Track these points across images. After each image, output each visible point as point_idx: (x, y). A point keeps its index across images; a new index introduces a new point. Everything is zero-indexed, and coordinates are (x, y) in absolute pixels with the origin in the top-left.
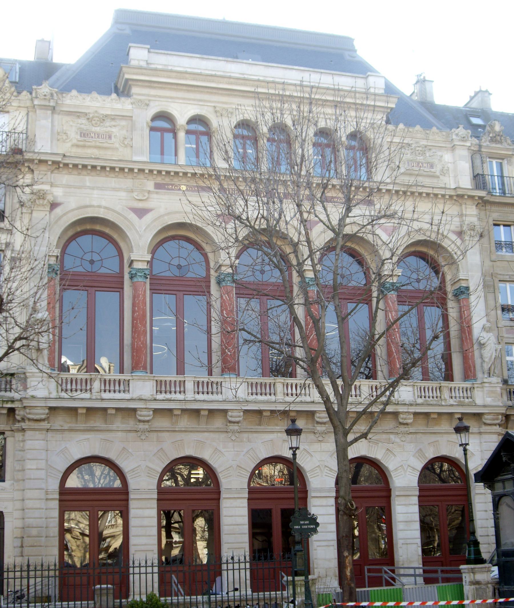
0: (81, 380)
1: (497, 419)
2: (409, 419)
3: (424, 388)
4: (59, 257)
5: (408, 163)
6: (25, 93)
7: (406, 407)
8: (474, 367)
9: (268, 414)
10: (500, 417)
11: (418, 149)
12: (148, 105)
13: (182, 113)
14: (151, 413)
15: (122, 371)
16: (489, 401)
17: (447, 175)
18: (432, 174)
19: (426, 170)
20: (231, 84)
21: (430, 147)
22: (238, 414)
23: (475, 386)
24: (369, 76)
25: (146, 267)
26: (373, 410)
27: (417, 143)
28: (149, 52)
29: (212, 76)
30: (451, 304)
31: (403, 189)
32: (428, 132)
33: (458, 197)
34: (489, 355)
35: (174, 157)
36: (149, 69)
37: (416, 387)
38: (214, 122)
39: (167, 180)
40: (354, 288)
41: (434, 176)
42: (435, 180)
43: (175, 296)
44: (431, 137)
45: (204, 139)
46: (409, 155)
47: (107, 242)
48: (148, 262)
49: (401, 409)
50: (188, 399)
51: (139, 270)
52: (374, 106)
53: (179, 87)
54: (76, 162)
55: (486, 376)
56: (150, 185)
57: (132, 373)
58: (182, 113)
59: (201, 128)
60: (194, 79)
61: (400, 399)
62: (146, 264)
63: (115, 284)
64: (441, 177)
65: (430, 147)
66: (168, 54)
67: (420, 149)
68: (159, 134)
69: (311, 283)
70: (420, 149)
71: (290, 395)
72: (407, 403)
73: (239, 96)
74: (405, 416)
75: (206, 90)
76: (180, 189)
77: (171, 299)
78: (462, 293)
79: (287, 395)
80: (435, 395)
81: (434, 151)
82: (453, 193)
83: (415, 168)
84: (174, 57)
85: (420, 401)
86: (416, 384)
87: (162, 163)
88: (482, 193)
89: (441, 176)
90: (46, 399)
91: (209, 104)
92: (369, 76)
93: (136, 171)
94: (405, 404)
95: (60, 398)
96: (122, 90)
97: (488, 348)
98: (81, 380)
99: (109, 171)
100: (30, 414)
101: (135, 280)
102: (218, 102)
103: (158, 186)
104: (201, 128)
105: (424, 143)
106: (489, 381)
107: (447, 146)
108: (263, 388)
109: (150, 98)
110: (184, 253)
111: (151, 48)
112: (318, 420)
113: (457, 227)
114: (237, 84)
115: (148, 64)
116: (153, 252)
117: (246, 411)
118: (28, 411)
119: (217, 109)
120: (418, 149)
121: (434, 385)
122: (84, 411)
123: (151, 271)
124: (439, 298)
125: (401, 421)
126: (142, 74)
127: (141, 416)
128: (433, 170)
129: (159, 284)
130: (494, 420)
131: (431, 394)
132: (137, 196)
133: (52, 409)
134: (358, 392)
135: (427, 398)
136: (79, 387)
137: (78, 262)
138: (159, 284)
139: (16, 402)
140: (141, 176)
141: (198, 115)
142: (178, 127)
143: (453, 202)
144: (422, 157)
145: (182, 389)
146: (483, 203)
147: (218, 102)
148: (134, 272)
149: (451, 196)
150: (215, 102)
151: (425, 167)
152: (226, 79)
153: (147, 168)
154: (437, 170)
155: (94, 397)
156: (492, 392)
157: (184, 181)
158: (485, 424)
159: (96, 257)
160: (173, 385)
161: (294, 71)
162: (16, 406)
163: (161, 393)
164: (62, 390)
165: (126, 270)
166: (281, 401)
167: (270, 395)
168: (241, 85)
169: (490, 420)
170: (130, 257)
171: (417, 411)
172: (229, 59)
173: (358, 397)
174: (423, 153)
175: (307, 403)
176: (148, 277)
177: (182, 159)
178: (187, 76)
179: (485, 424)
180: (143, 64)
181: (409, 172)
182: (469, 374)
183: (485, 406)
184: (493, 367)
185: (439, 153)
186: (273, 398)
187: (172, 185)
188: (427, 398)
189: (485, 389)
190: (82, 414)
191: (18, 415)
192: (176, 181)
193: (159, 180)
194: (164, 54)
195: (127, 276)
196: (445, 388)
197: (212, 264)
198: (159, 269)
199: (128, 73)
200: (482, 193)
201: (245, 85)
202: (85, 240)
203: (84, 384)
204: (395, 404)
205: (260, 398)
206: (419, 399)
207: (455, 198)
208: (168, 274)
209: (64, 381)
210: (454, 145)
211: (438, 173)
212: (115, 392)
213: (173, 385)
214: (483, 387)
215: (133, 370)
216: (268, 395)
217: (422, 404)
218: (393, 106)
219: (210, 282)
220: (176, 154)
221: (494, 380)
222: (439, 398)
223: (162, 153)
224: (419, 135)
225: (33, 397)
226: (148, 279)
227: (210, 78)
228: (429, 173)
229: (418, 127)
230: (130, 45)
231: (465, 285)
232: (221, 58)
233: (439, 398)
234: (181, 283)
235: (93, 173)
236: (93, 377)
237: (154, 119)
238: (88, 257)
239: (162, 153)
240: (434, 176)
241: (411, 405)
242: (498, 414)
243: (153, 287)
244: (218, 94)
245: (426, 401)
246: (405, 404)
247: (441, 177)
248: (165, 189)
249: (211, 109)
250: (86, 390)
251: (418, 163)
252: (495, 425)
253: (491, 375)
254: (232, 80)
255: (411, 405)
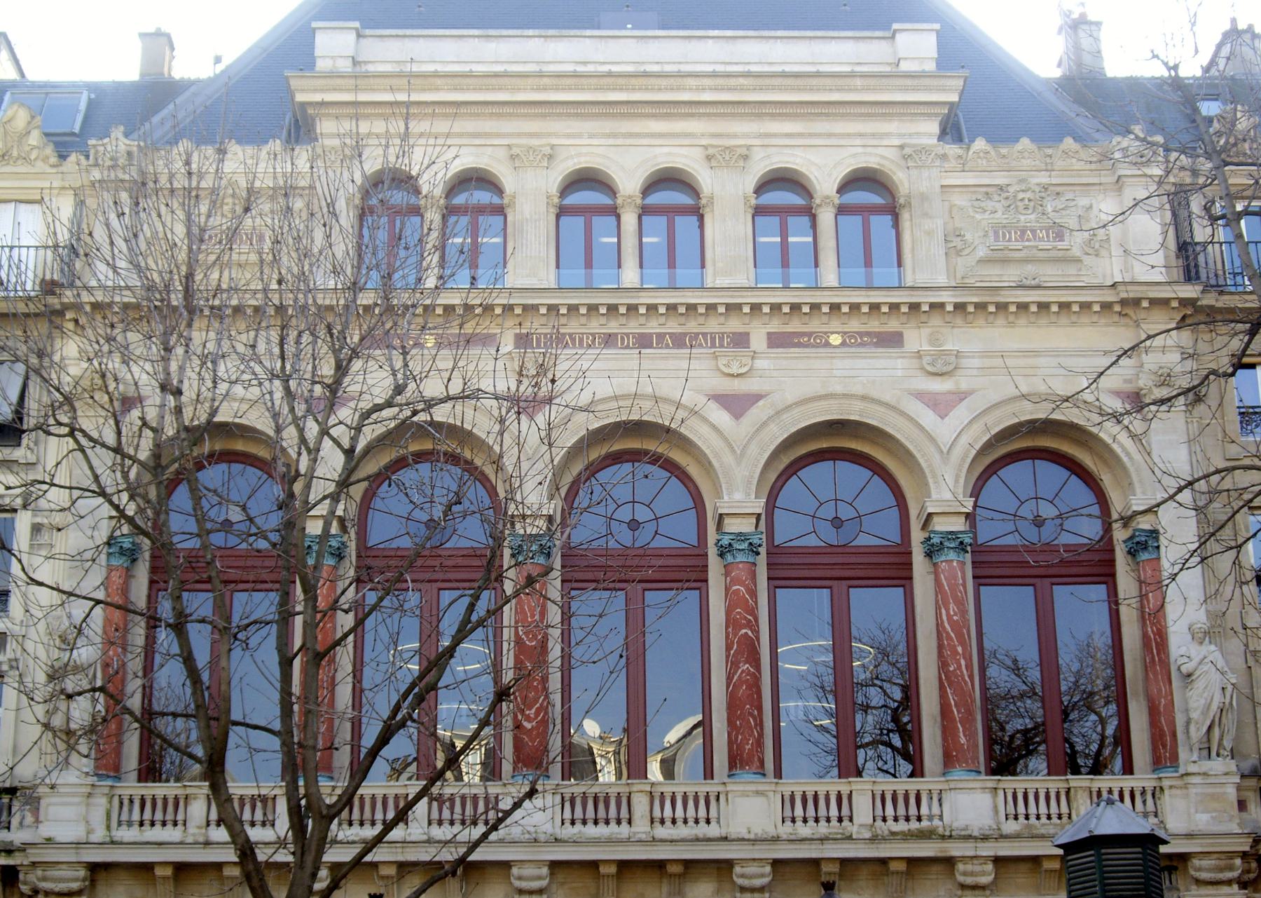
0: (373, 797)
1: (1231, 868)
2: (984, 873)
3: (1058, 794)
4: (763, 517)
5: (996, 233)
6: (73, 158)
7: (970, 844)
8: (1174, 735)
9: (902, 866)
10: (1238, 862)
11: (1021, 195)
12: (746, 158)
13: (825, 171)
14: (768, 869)
15: (709, 773)
16: (1202, 821)
17: (1104, 253)
18: (1060, 254)
19: (1042, 245)
20: (545, 89)
21: (1059, 189)
22: (536, 872)
23: (1166, 783)
24: (895, 31)
25: (962, 529)
26: (376, 859)
27: (1021, 181)
28: (359, 36)
29: (496, 75)
30: (1126, 583)
31: (975, 300)
32: (1049, 151)
33: (1126, 304)
34: (1203, 701)
35: (896, 270)
36: (359, 75)
37: (1001, 793)
38: (706, 180)
39: (795, 326)
40: (1068, 548)
41: (1066, 259)
42: (1072, 270)
43: (901, 589)
44: (1059, 164)
45: (881, 223)
46: (999, 215)
47: (1066, 473)
48: (967, 515)
49: (955, 849)
50: (413, 838)
51: (741, 537)
52: (408, 104)
53: (832, 110)
54: (1065, 297)
55: (1195, 757)
56: (758, 341)
57: (944, 774)
58: (825, 171)
59: (875, 199)
60: (455, 89)
61: (955, 825)
62: (963, 519)
63: (687, 572)
64: (1087, 260)
65: (1059, 189)
66: (405, 36)
67: (1028, 195)
68: (857, 220)
69: (736, 546)
70: (1028, 195)
71: (668, 823)
72: (976, 834)
73: (569, 115)
74: (969, 867)
75: (489, 110)
76: (827, 344)
77: (820, 599)
78: (1146, 543)
79: (662, 822)
80: (1032, 809)
81: (1070, 196)
82: (1110, 297)
83: (1014, 245)
84: (421, 40)
85: (1011, 827)
86: (1001, 785)
87: (589, 288)
88: (1189, 291)
89: (1085, 258)
90: (78, 844)
91: (885, 142)
92: (895, 31)
93: (925, 308)
94: (969, 837)
95: (113, 842)
96: (299, 128)
97: (1199, 685)
98: (165, 799)
99: (770, 314)
100: (44, 879)
101: (729, 558)
102: (519, 135)
103: (776, 341)
104: (875, 199)
105: (1043, 179)
106: (1203, 769)
107: (1103, 180)
108: (601, 806)
109: (749, 142)
110: (645, 490)
111: (364, 27)
112: (740, 881)
113: (1126, 381)
114: (557, 89)
115: (355, 63)
116: (976, 493)
117: (555, 866)
118: (39, 873)
119: (515, 151)
120: (1021, 195)
121: (1050, 785)
122: (168, 872)
123: (975, 538)
124: (1096, 566)
125: (961, 879)
126: (614, 89)
127: (520, 878)
128: (1060, 245)
129: (789, 568)
130: (1221, 870)
131: (1043, 809)
132: (728, 366)
133: (96, 870)
134: (845, 811)
135: (1033, 820)
136: (159, 816)
137: (805, 524)
138: (789, 568)
139: (17, 854)
140: (936, 320)
141: (476, 170)
142: (902, 201)
143: (1116, 318)
144: (1033, 217)
145: (624, 813)
146: (1193, 316)
147: (519, 135)
148: (936, 540)
149: (1106, 306)
150: (901, 135)
151: (1041, 240)
152: (530, 81)
153: (948, 298)
154: (1075, 243)
155: (190, 840)
156: (1214, 797)
157: (835, 324)
158: (1199, 882)
159: (642, 514)
160: (912, 801)
161: (710, 41)
162: (18, 862)
163: (350, 824)
164: (120, 824)
165: (917, 536)
166: (643, 837)
167: (619, 822)
168: (569, 89)
169: (1209, 870)
170: (716, 508)
171: (1002, 853)
172: (551, 32)
173: (846, 823)
174: (1037, 205)
175: (709, 840)
176: (969, 548)
177: (829, 276)
178: (439, 82)
179: (1199, 882)
180: (345, 66)
181: (999, 255)
182: (1164, 755)
183: (1190, 836)
184: (1216, 732)
185: (1083, 202)
186: (624, 830)
187: (809, 335)
188: (1033, 820)
189: (1193, 791)
190: (164, 878)
191: (25, 883)
192: (815, 325)
193: (776, 326)
194: (397, 36)
195: (712, 552)
196: (1080, 792)
197: (913, 512)
198: (789, 530)
199: (303, 91)
200: (1189, 291)
201: (578, 88)
202: (1017, 473)
203: (170, 808)
204: (943, 837)
205: (591, 830)
206: (1011, 822)
207: (1117, 308)
208: (812, 541)
209: (126, 802)
210: (1119, 177)
211: (1076, 252)
212: (596, 822)
213: (912, 801)
214: (1186, 786)
215: (730, 769)
216: (613, 824)
217: (1016, 836)
218: (954, 98)
219: (910, 553)
220: (900, 265)
221: (1218, 765)
222: (1065, 819)
223: (868, 263)
224: (1027, 163)
225: (49, 840)
226: (968, 556)
227: (494, 81)
228: (1053, 254)
229: (1025, 142)
230: (314, 25)
231: (1147, 527)
232: (531, 32)
233: (1065, 819)
234: (1006, 558)
235: (1043, 321)
236: (1072, 784)
237: (760, 189)
238: (1027, 511)
239: (868, 263)
240: (1066, 259)
241: (985, 838)
242: (1231, 855)
243: (980, 572)
244: (517, 115)
245: (1028, 826)
246: (969, 837)
247: (1087, 260)
248: (799, 345)
249: (502, 153)
250: (175, 824)
251: (1023, 232)
252: (1229, 882)
253: (1214, 754)
254: (546, 80)
255: (985, 838)
